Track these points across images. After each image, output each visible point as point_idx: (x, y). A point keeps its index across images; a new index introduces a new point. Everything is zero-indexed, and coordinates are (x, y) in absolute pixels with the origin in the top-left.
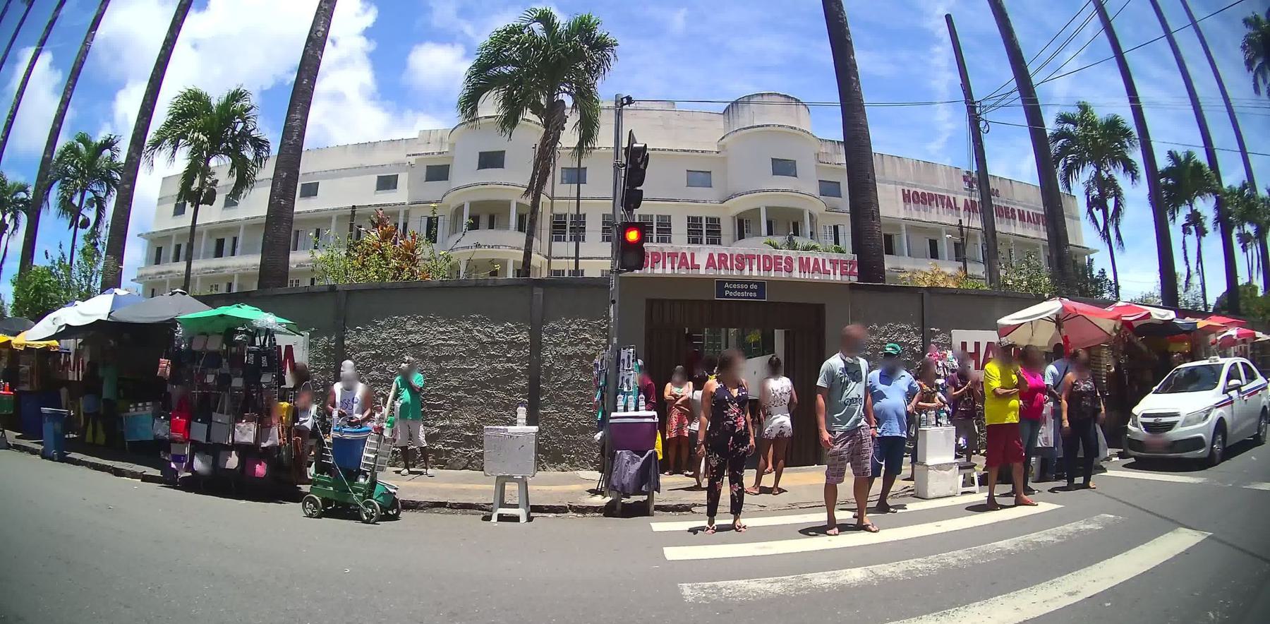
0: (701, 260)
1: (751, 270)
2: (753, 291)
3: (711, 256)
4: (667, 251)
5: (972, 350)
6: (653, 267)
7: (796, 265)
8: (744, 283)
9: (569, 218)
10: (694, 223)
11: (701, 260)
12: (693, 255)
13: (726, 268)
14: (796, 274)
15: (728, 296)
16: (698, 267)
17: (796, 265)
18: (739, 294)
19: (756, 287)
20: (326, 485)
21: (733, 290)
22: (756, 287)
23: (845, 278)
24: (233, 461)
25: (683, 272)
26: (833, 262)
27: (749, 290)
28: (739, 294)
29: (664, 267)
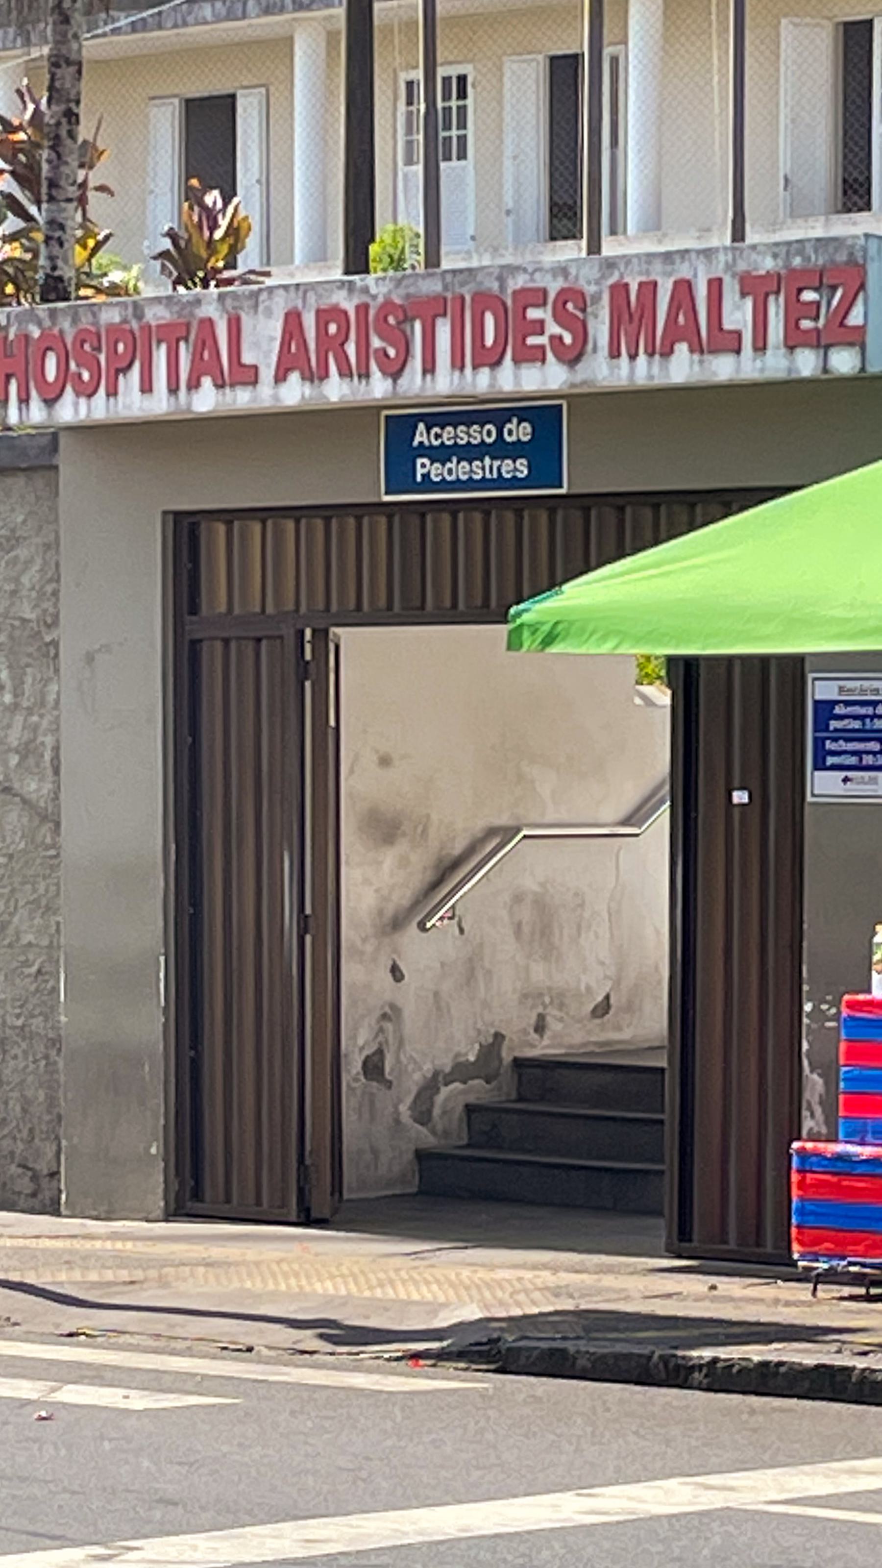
1: (429, 368)
2: (514, 451)
13: (345, 372)
14: (604, 371)
15: (428, 484)
19: (519, 432)
21: (441, 454)
23: (806, 363)
25: (206, 400)
27: (501, 450)
29: (147, 387)
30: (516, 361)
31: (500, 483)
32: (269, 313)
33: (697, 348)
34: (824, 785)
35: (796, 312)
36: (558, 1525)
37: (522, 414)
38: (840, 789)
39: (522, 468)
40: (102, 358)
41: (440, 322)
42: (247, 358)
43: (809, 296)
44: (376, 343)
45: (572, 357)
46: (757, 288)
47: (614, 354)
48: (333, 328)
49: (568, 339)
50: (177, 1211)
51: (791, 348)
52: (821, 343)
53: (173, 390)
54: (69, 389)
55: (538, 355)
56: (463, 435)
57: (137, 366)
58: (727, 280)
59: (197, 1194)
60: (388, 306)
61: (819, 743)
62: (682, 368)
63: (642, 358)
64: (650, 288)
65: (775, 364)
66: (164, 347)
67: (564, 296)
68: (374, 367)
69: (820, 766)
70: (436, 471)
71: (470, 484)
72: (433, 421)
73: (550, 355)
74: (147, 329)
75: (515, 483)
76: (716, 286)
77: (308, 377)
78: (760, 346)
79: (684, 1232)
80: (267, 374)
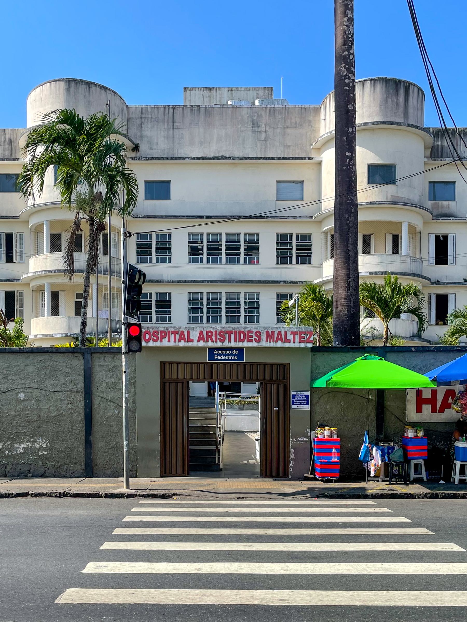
0: (195, 335)
1: (230, 341)
2: (235, 355)
3: (201, 333)
4: (170, 330)
6: (161, 341)
7: (264, 337)
8: (228, 350)
9: (242, 257)
11: (195, 335)
12: (188, 333)
13: (212, 341)
14: (264, 344)
15: (217, 359)
16: (192, 341)
17: (264, 337)
18: (224, 358)
20: (311, 334)
21: (220, 355)
23: (303, 345)
25: (182, 344)
26: (294, 334)
27: (232, 355)
28: (224, 358)
29: (169, 341)
30: (247, 341)
32: (196, 331)
34: (294, 407)
35: (300, 337)
36: (347, 529)
37: (236, 350)
39: (236, 358)
41: (232, 335)
42: (191, 338)
43: (303, 335)
44: (218, 337)
45: (258, 341)
46: (294, 334)
47: (267, 341)
48: (163, 334)
50: (162, 476)
51: (300, 343)
52: (306, 342)
53: (175, 341)
55: (252, 341)
56: (227, 352)
57: (167, 337)
58: (288, 332)
59: (165, 473)
60: (221, 332)
61: (293, 401)
62: (279, 344)
63: (272, 342)
64: (273, 332)
65: (297, 345)
66: (173, 335)
67: (257, 332)
68: (218, 341)
69: (293, 404)
70: (219, 358)
72: (217, 350)
73: (254, 341)
74: (169, 332)
75: (234, 360)
76: (286, 333)
78: (294, 342)
79: (266, 475)
80: (195, 341)
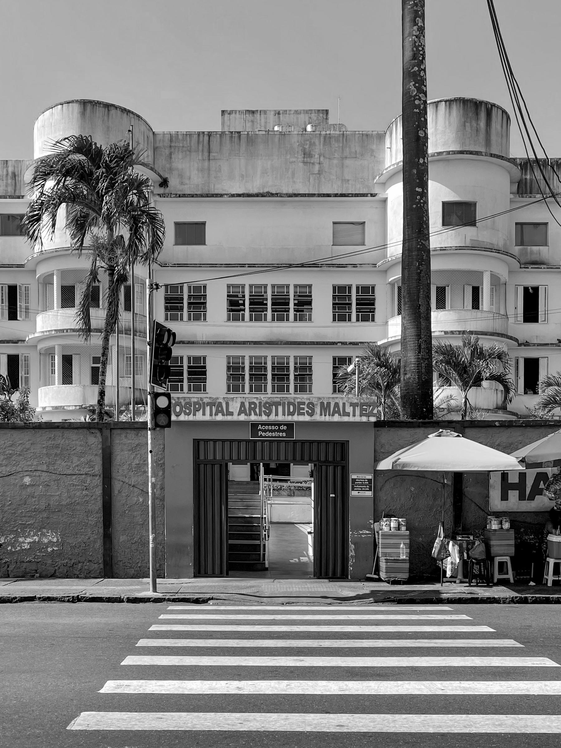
0: (235, 407)
1: (277, 415)
2: (283, 431)
3: (242, 404)
4: (205, 400)
5: (516, 480)
7: (318, 410)
8: (275, 425)
10: (341, 296)
11: (235, 407)
12: (227, 404)
13: (256, 414)
14: (317, 417)
15: (261, 436)
16: (231, 414)
17: (318, 410)
18: (274, 434)
19: (285, 428)
21: (265, 431)
22: (285, 428)
23: (364, 419)
24: (421, 52)
25: (220, 418)
26: (354, 405)
29: (204, 414)
30: (298, 415)
31: (279, 437)
33: (340, 415)
34: (354, 493)
35: (362, 410)
37: (285, 425)
38: (358, 494)
39: (284, 434)
40: (192, 408)
43: (364, 407)
44: (263, 409)
45: (311, 415)
47: (321, 415)
48: (197, 406)
49: (310, 411)
50: (195, 577)
54: (183, 414)
55: (303, 414)
58: (346, 403)
59: (199, 573)
60: (267, 403)
62: (336, 418)
63: (327, 416)
64: (329, 404)
65: (357, 419)
66: (209, 407)
67: (309, 403)
68: (263, 414)
69: (353, 490)
70: (263, 434)
71: (272, 437)
75: (283, 437)
77: (246, 415)
78: (354, 415)
80: (236, 414)
